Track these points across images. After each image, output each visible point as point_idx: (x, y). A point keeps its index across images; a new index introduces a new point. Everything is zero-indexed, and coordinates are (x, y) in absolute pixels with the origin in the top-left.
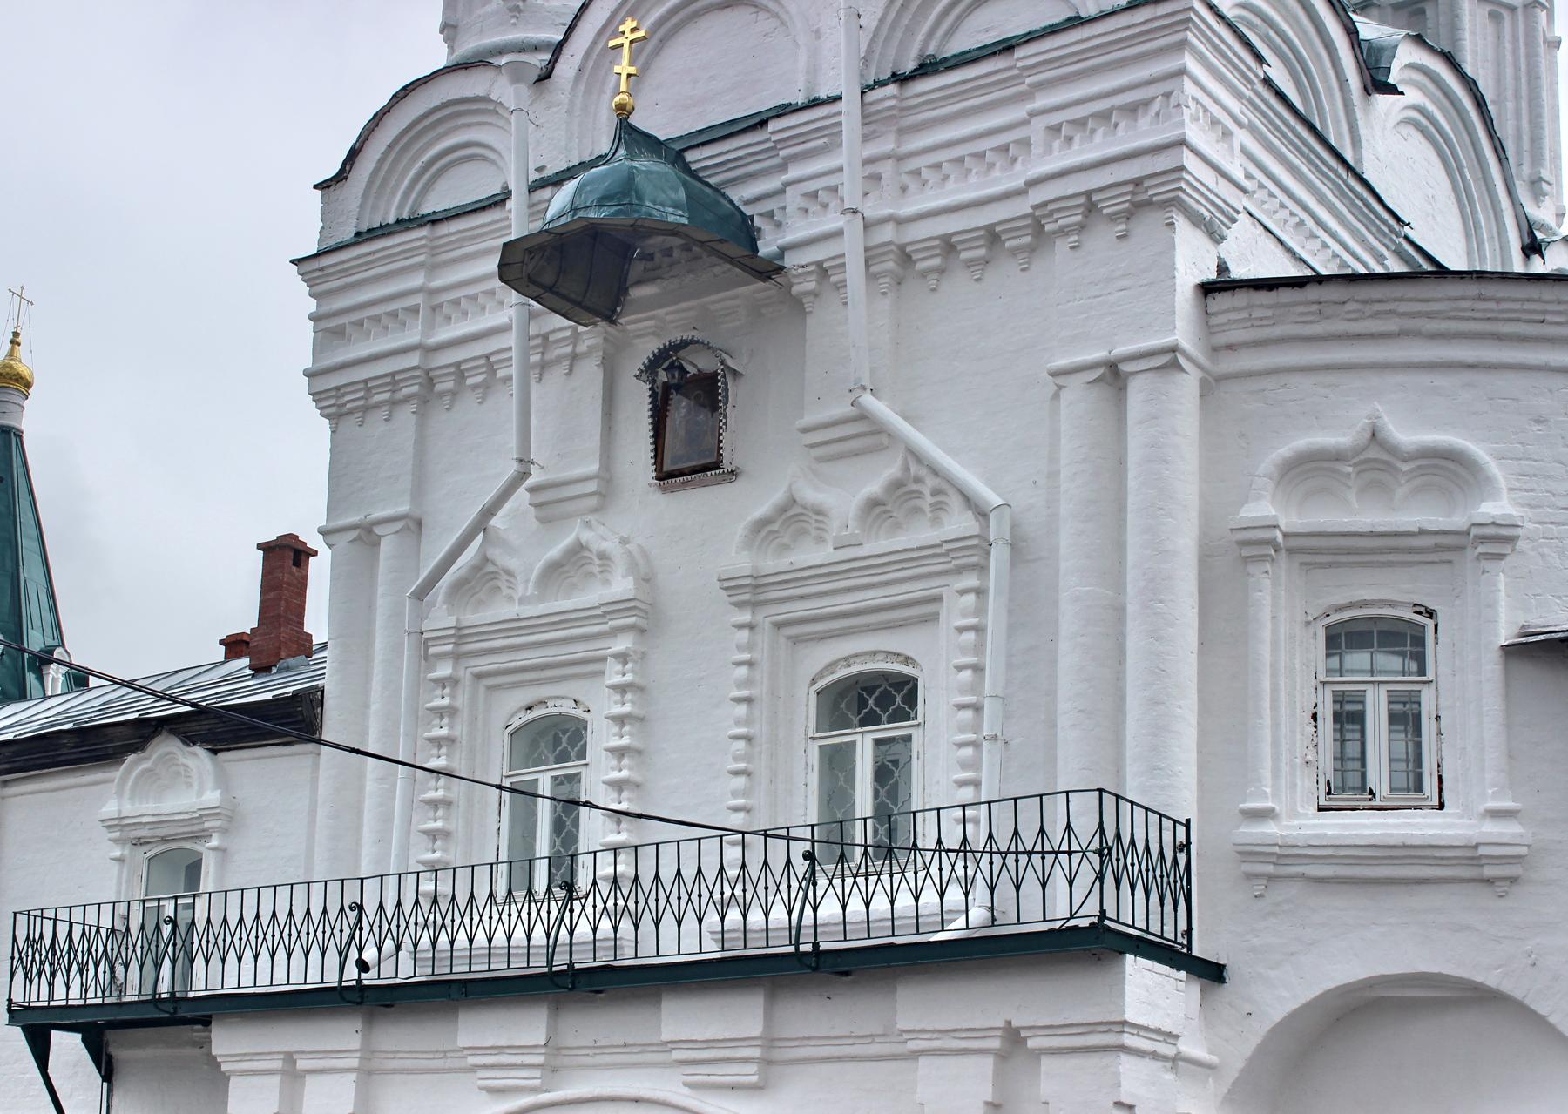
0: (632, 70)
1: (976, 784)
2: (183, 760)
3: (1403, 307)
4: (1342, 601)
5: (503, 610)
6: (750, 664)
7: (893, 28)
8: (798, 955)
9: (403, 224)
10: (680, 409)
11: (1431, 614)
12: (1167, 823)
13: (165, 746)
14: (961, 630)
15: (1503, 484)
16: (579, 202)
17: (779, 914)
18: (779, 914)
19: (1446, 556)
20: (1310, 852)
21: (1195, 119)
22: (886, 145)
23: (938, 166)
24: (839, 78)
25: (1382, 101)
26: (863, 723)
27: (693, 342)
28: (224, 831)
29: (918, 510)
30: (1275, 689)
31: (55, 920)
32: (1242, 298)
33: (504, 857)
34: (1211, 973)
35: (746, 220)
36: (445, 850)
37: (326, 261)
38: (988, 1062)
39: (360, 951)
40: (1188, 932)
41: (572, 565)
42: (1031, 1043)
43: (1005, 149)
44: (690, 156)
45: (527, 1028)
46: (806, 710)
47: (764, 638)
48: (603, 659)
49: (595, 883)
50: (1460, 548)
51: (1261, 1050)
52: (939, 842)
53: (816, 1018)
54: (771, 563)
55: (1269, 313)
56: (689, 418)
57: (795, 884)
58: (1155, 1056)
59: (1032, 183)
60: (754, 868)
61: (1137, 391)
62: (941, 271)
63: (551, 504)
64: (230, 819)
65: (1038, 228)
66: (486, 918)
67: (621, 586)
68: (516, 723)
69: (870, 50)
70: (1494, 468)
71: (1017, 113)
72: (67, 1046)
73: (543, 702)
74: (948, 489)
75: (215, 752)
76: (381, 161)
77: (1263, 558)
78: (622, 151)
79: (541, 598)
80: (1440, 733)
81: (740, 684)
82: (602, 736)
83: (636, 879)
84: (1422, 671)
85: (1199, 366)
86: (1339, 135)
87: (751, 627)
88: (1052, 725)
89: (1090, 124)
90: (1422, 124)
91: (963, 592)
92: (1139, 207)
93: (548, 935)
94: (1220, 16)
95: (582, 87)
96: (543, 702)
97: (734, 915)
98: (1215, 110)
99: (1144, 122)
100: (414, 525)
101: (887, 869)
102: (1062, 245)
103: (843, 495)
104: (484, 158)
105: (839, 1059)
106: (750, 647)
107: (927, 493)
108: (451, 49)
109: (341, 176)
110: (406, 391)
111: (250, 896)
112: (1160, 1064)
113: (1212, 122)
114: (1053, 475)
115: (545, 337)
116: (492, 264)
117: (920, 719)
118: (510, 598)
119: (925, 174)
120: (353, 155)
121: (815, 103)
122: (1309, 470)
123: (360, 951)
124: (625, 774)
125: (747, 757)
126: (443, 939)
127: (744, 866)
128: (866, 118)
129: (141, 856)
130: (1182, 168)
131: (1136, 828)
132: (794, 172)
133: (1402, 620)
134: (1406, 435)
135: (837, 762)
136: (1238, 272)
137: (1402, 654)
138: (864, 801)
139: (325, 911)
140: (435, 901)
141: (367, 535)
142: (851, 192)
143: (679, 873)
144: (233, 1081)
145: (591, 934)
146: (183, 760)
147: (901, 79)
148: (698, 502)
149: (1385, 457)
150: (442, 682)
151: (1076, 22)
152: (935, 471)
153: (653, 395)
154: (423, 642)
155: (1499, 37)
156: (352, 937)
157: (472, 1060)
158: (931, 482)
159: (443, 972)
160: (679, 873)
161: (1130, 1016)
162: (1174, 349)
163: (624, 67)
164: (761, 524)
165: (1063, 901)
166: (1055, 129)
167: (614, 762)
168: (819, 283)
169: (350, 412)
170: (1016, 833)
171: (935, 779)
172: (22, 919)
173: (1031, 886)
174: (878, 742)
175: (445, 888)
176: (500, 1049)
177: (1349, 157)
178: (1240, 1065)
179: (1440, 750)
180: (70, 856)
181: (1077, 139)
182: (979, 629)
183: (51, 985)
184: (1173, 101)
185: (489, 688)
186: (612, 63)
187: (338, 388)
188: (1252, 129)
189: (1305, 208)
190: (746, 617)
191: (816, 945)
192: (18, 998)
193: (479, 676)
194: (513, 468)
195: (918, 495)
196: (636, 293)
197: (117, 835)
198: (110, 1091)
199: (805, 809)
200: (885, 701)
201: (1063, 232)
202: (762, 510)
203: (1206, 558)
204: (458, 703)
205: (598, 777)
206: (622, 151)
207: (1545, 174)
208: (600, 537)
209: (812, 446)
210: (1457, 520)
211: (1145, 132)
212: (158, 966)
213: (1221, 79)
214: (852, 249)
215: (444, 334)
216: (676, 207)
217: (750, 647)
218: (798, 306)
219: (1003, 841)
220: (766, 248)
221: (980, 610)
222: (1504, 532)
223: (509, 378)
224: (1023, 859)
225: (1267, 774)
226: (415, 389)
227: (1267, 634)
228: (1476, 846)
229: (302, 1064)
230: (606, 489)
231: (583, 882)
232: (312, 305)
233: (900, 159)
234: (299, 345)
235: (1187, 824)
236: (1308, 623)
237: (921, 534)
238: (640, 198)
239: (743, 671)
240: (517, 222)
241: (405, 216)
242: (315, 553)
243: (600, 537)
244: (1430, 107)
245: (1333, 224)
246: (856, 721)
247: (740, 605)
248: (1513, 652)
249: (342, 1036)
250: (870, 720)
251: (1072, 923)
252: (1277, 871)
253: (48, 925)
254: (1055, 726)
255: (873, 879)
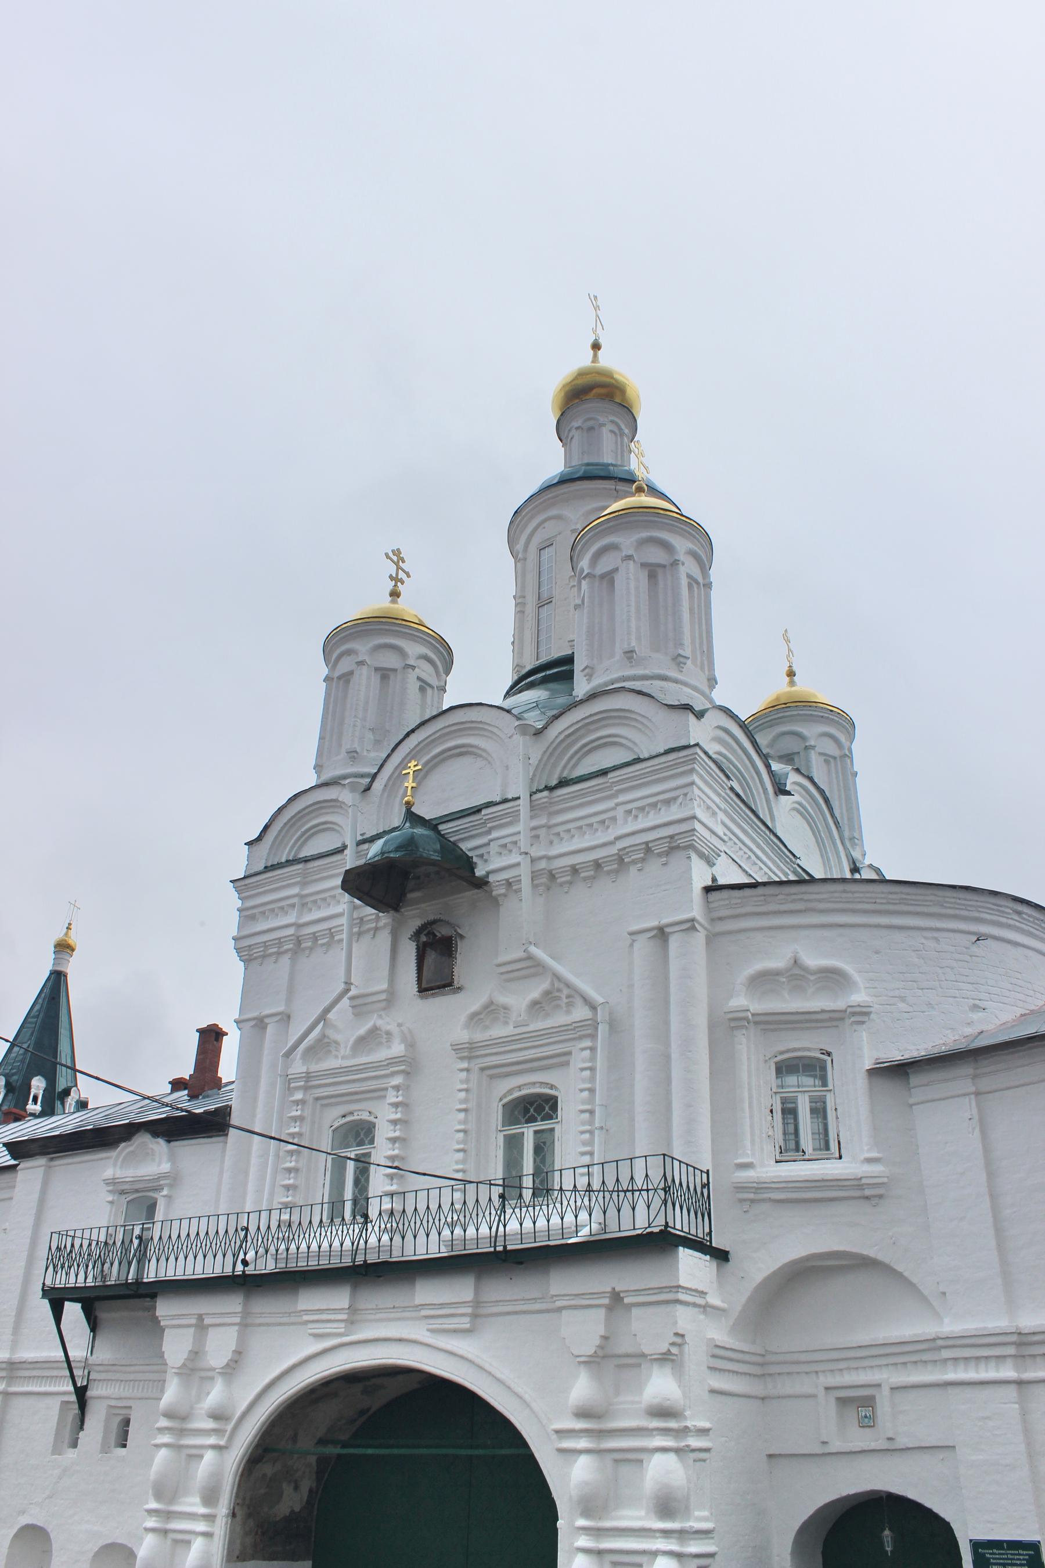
0: (414, 785)
1: (591, 1154)
2: (151, 1146)
3: (806, 897)
4: (783, 1049)
5: (332, 1063)
6: (467, 1090)
7: (545, 765)
8: (495, 1252)
9: (289, 863)
10: (431, 957)
11: (829, 1054)
12: (698, 1172)
13: (144, 1139)
14: (582, 1069)
15: (861, 985)
16: (386, 849)
17: (484, 1230)
18: (484, 1230)
19: (834, 1023)
20: (773, 1185)
21: (699, 806)
22: (543, 821)
23: (569, 831)
24: (518, 787)
25: (783, 798)
26: (527, 1122)
27: (440, 920)
28: (171, 1186)
29: (558, 1006)
30: (750, 1097)
31: (74, 1237)
32: (725, 894)
33: (326, 1200)
34: (721, 1256)
35: (469, 859)
36: (293, 1196)
37: (247, 881)
38: (602, 1313)
39: (245, 1254)
40: (710, 1233)
41: (371, 1038)
42: (626, 1300)
43: (603, 822)
44: (441, 827)
45: (337, 1299)
46: (496, 1115)
47: (474, 1076)
48: (386, 1089)
49: (380, 1214)
50: (842, 1019)
51: (750, 1299)
52: (575, 1186)
53: (506, 1291)
54: (479, 1036)
55: (739, 901)
56: (437, 962)
57: (493, 1212)
58: (695, 1305)
59: (618, 838)
60: (471, 1203)
61: (674, 942)
62: (570, 883)
63: (361, 1006)
64: (175, 1179)
65: (620, 860)
66: (318, 1234)
67: (397, 1049)
68: (336, 1124)
69: (534, 775)
70: (856, 977)
71: (610, 804)
72: (73, 1311)
73: (351, 1113)
74: (575, 994)
75: (169, 1141)
76: (280, 831)
77: (743, 1027)
78: (408, 824)
79: (354, 1056)
80: (837, 1118)
81: (461, 1102)
82: (384, 1132)
83: (404, 1211)
84: (825, 1084)
85: (705, 929)
86: (764, 814)
87: (468, 1070)
88: (632, 1120)
89: (647, 809)
90: (800, 810)
91: (583, 1049)
92: (673, 849)
93: (353, 1244)
94: (710, 757)
95: (386, 794)
96: (351, 1113)
97: (458, 1231)
98: (708, 802)
99: (674, 808)
100: (286, 1018)
101: (545, 1202)
102: (633, 870)
103: (518, 999)
104: (333, 830)
105: (516, 1313)
106: (467, 1081)
107: (564, 997)
108: (319, 777)
109: (259, 839)
110: (286, 947)
111: (185, 1223)
112: (697, 1310)
113: (708, 809)
114: (631, 986)
115: (361, 919)
116: (338, 881)
117: (559, 1119)
118: (336, 1057)
119: (562, 834)
120: (266, 828)
121: (505, 801)
122: (764, 981)
123: (245, 1254)
124: (396, 1152)
125: (464, 1142)
126: (293, 1247)
127: (465, 1202)
128: (532, 808)
129: (124, 1200)
130: (694, 830)
131: (678, 1173)
132: (495, 834)
133: (814, 1058)
134: (812, 961)
135: (513, 1144)
136: (721, 881)
137: (815, 1077)
138: (528, 1165)
139: (227, 1231)
140: (290, 1225)
141: (260, 1024)
142: (524, 844)
143: (428, 1207)
144: (167, 1331)
145: (376, 1242)
146: (151, 1146)
147: (550, 789)
148: (440, 1004)
149: (802, 973)
150: (297, 1103)
151: (638, 760)
152: (568, 985)
153: (418, 949)
154: (288, 1080)
155: (829, 771)
156: (241, 1246)
157: (306, 1318)
158: (566, 991)
159: (292, 1265)
160: (428, 1207)
161: (682, 1283)
162: (693, 920)
163: (410, 783)
164: (474, 1015)
165: (640, 1218)
166: (629, 812)
167: (391, 1146)
168: (507, 890)
169: (256, 958)
170: (618, 1180)
171: (568, 1151)
172: (55, 1236)
173: (626, 1209)
174: (536, 1132)
175: (295, 1218)
176: (321, 1311)
177: (770, 825)
178: (739, 1308)
179: (838, 1126)
180: (84, 1201)
181: (640, 816)
182: (592, 1069)
183: (73, 1245)
184: (688, 797)
185: (322, 1105)
186: (402, 782)
187: (250, 946)
188: (725, 812)
189: (751, 850)
190: (465, 1065)
191: (505, 1247)
192: (48, 1282)
193: (317, 1099)
194: (342, 986)
195: (559, 998)
196: (411, 896)
197: (111, 1188)
198: (94, 1337)
199: (497, 1172)
200: (539, 1109)
201: (634, 862)
202: (475, 1007)
203: (712, 1027)
204: (305, 1114)
205: (381, 1151)
206: (408, 824)
207: (856, 835)
208: (387, 1023)
209: (502, 974)
210: (840, 1004)
211: (675, 813)
212: (130, 1264)
213: (711, 787)
214: (524, 873)
215: (307, 918)
216: (435, 851)
217: (467, 1081)
218: (495, 902)
219: (610, 1185)
220: (479, 872)
221: (593, 1059)
222: (864, 1010)
223: (341, 940)
224: (622, 1194)
225: (748, 1143)
226: (291, 946)
227: (745, 1068)
228: (861, 1179)
229: (207, 1321)
230: (391, 998)
231: (373, 1213)
232: (239, 903)
233: (549, 827)
234: (231, 924)
235: (708, 1173)
236: (766, 1061)
237: (561, 1019)
238: (417, 847)
239: (463, 1094)
240: (350, 860)
241: (291, 858)
242: (227, 1034)
243: (387, 1023)
244: (804, 803)
245: (764, 858)
246: (523, 1120)
247: (462, 1059)
248: (873, 1072)
249: (232, 1304)
250: (531, 1120)
251: (649, 1230)
252: (755, 1196)
253: (70, 1239)
254: (634, 1120)
255: (537, 1208)
